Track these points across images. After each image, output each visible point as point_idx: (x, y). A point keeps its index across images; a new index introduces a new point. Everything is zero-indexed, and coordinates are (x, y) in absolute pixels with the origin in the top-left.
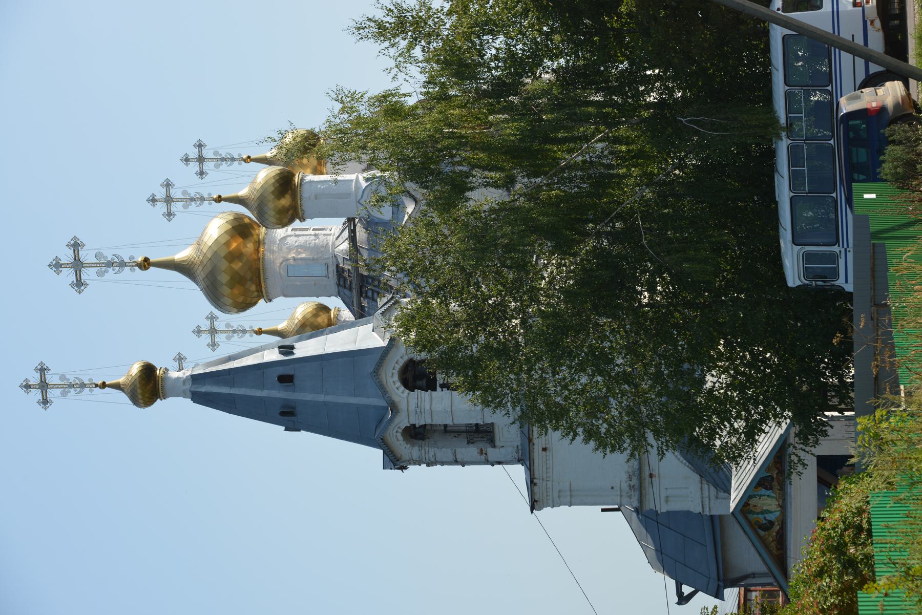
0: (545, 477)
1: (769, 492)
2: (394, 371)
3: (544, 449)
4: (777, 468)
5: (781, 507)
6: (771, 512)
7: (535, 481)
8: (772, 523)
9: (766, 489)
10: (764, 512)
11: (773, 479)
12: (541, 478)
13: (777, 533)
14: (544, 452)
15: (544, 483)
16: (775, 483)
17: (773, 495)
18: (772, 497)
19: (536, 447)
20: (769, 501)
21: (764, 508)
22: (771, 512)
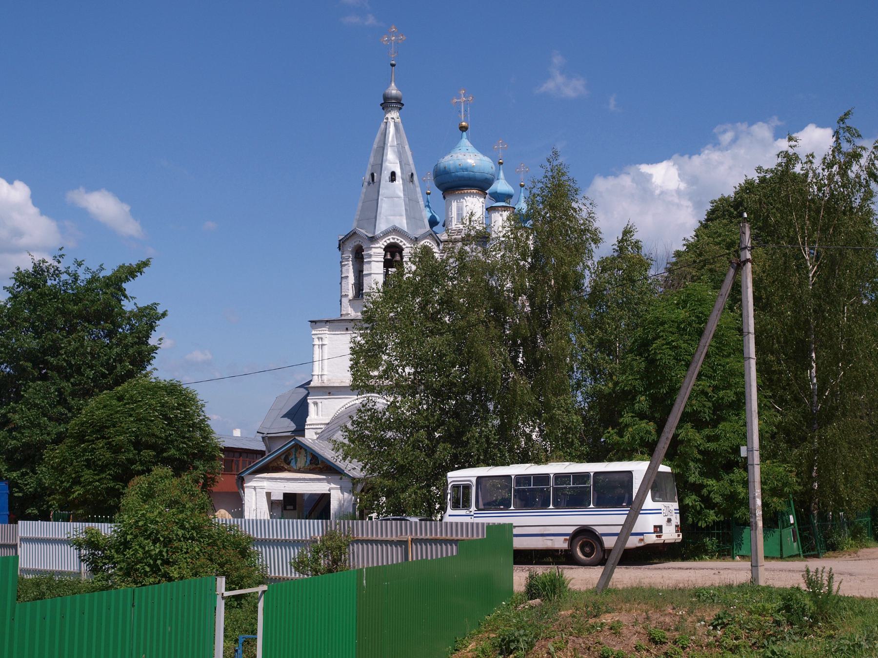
1: (308, 462)
4: (323, 468)
5: (299, 470)
6: (296, 463)
8: (289, 464)
9: (311, 460)
10: (296, 458)
11: (317, 465)
13: (283, 467)
16: (314, 466)
17: (307, 465)
18: (305, 464)
20: (303, 462)
21: (299, 459)
22: (296, 463)
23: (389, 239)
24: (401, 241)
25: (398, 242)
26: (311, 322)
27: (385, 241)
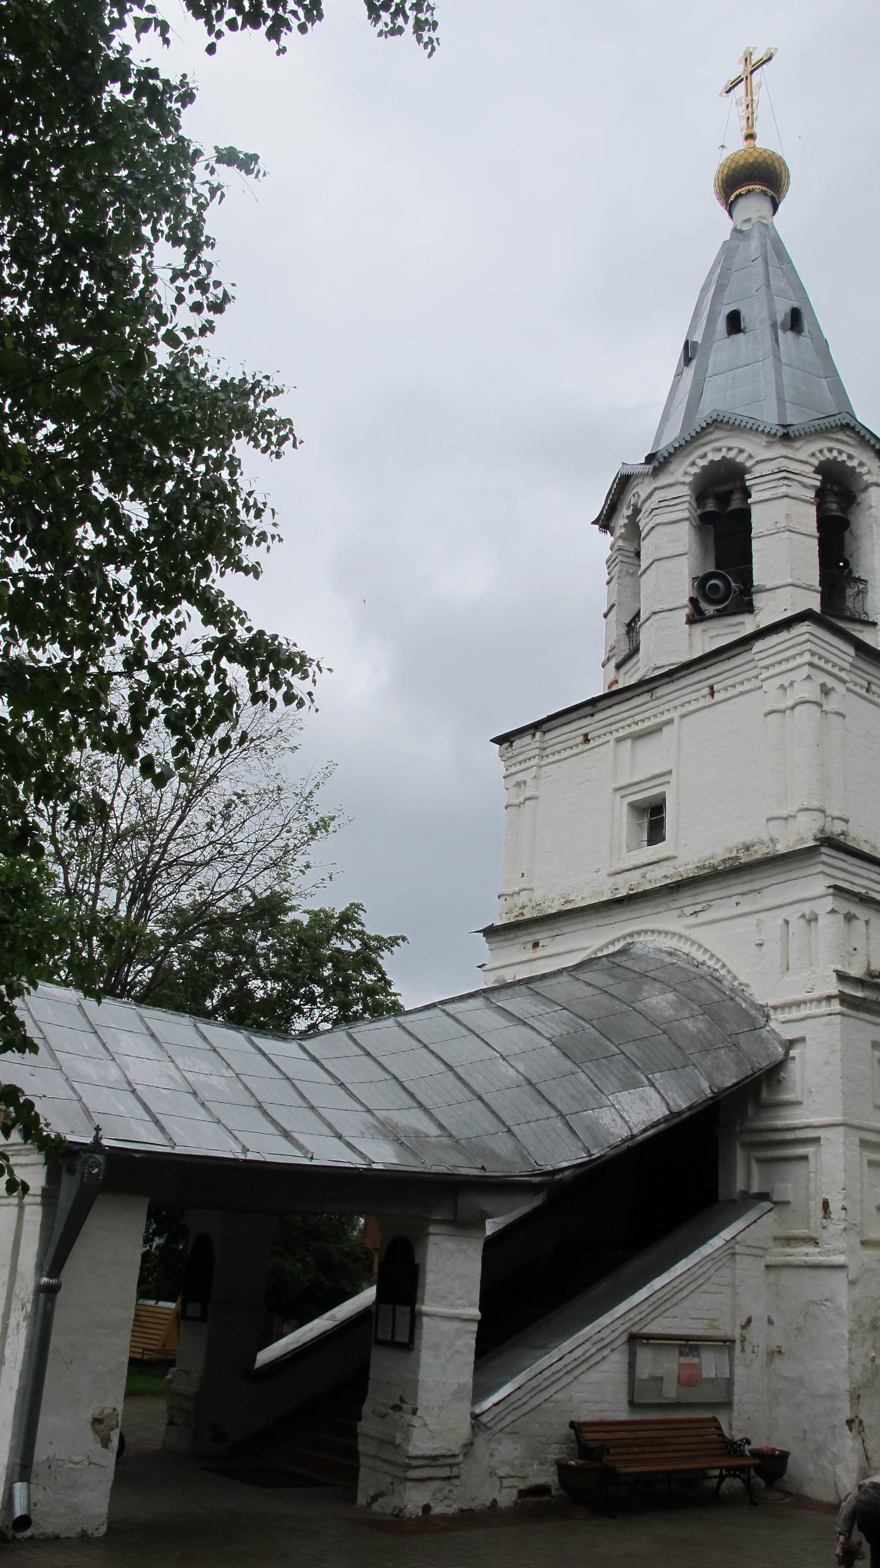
0: (548, 751)
2: (724, 450)
3: (586, 740)
7: (538, 734)
12: (545, 745)
14: (581, 739)
15: (537, 752)
19: (588, 721)
23: (704, 456)
24: (741, 451)
25: (731, 455)
26: (499, 740)
27: (821, 451)
